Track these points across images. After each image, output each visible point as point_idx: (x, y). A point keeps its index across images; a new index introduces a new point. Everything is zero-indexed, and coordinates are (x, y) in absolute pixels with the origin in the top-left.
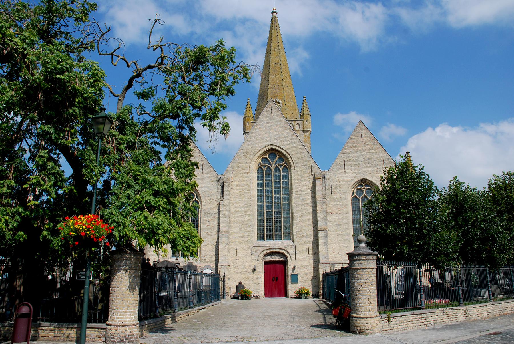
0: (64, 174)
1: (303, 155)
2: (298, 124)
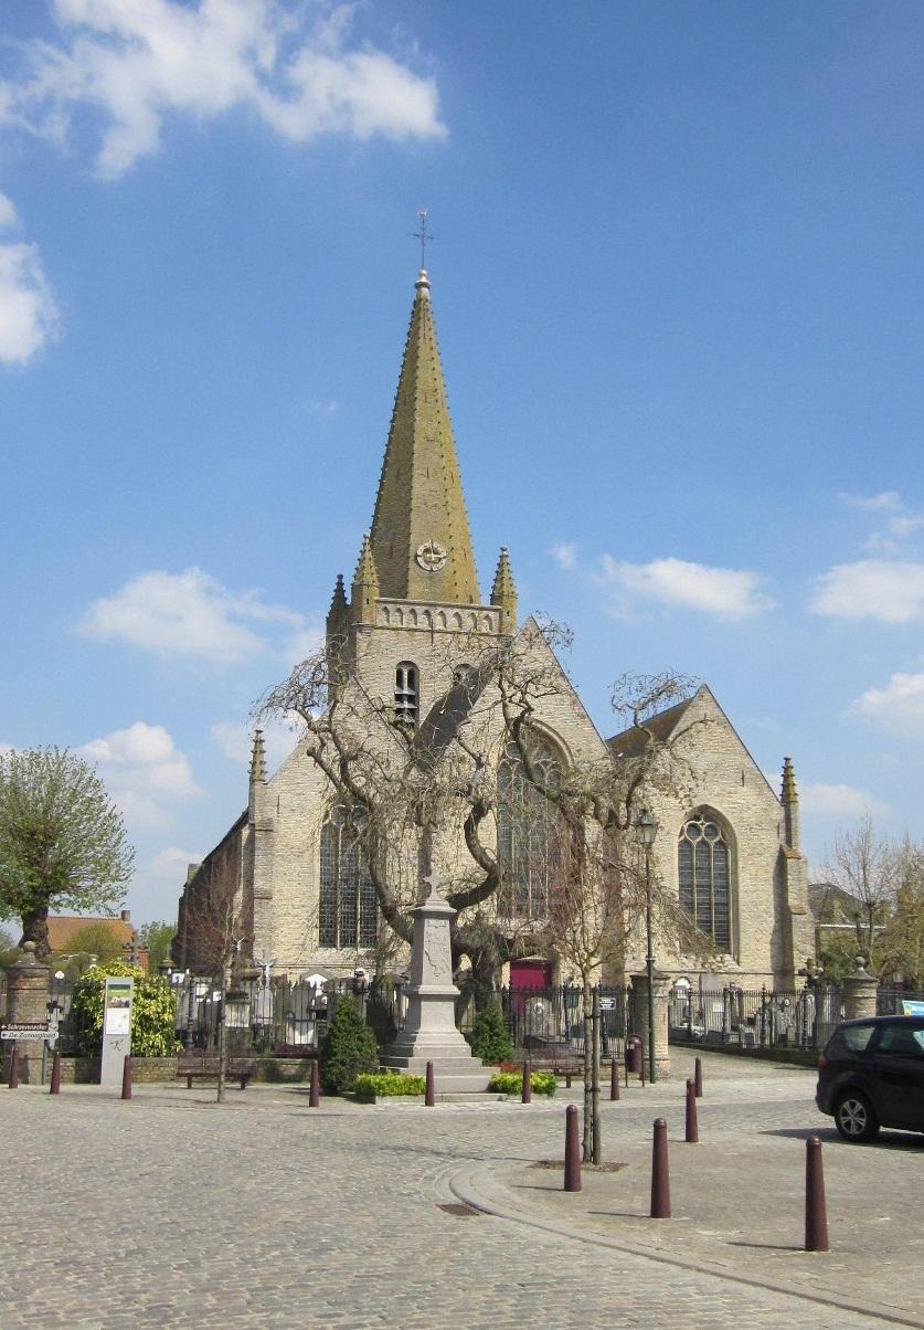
1: (593, 745)
2: (487, 617)
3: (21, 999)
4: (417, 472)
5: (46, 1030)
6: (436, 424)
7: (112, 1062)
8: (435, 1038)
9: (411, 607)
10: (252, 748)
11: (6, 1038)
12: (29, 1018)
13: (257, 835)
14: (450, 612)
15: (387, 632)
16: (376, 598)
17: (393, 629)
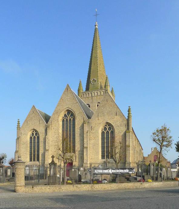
0: (168, 133)
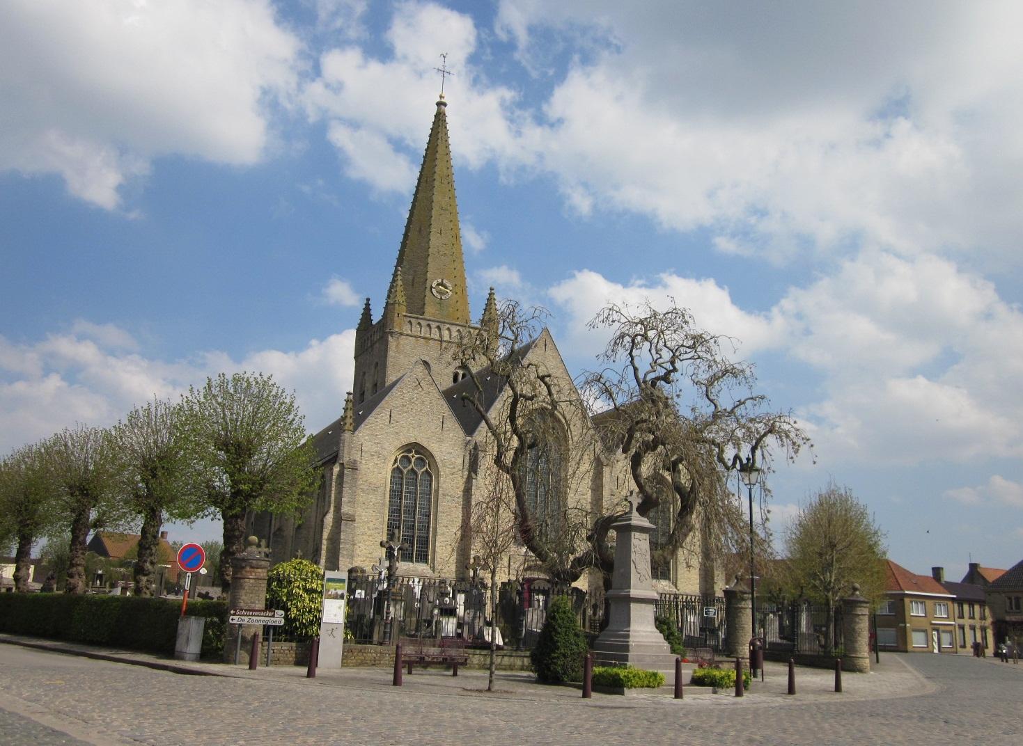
3: (246, 588)
4: (433, 230)
5: (273, 616)
6: (447, 199)
7: (331, 647)
8: (643, 636)
9: (428, 322)
10: (344, 406)
11: (234, 622)
12: (253, 605)
13: (346, 472)
14: (454, 329)
15: (410, 338)
16: (404, 314)
17: (415, 337)
